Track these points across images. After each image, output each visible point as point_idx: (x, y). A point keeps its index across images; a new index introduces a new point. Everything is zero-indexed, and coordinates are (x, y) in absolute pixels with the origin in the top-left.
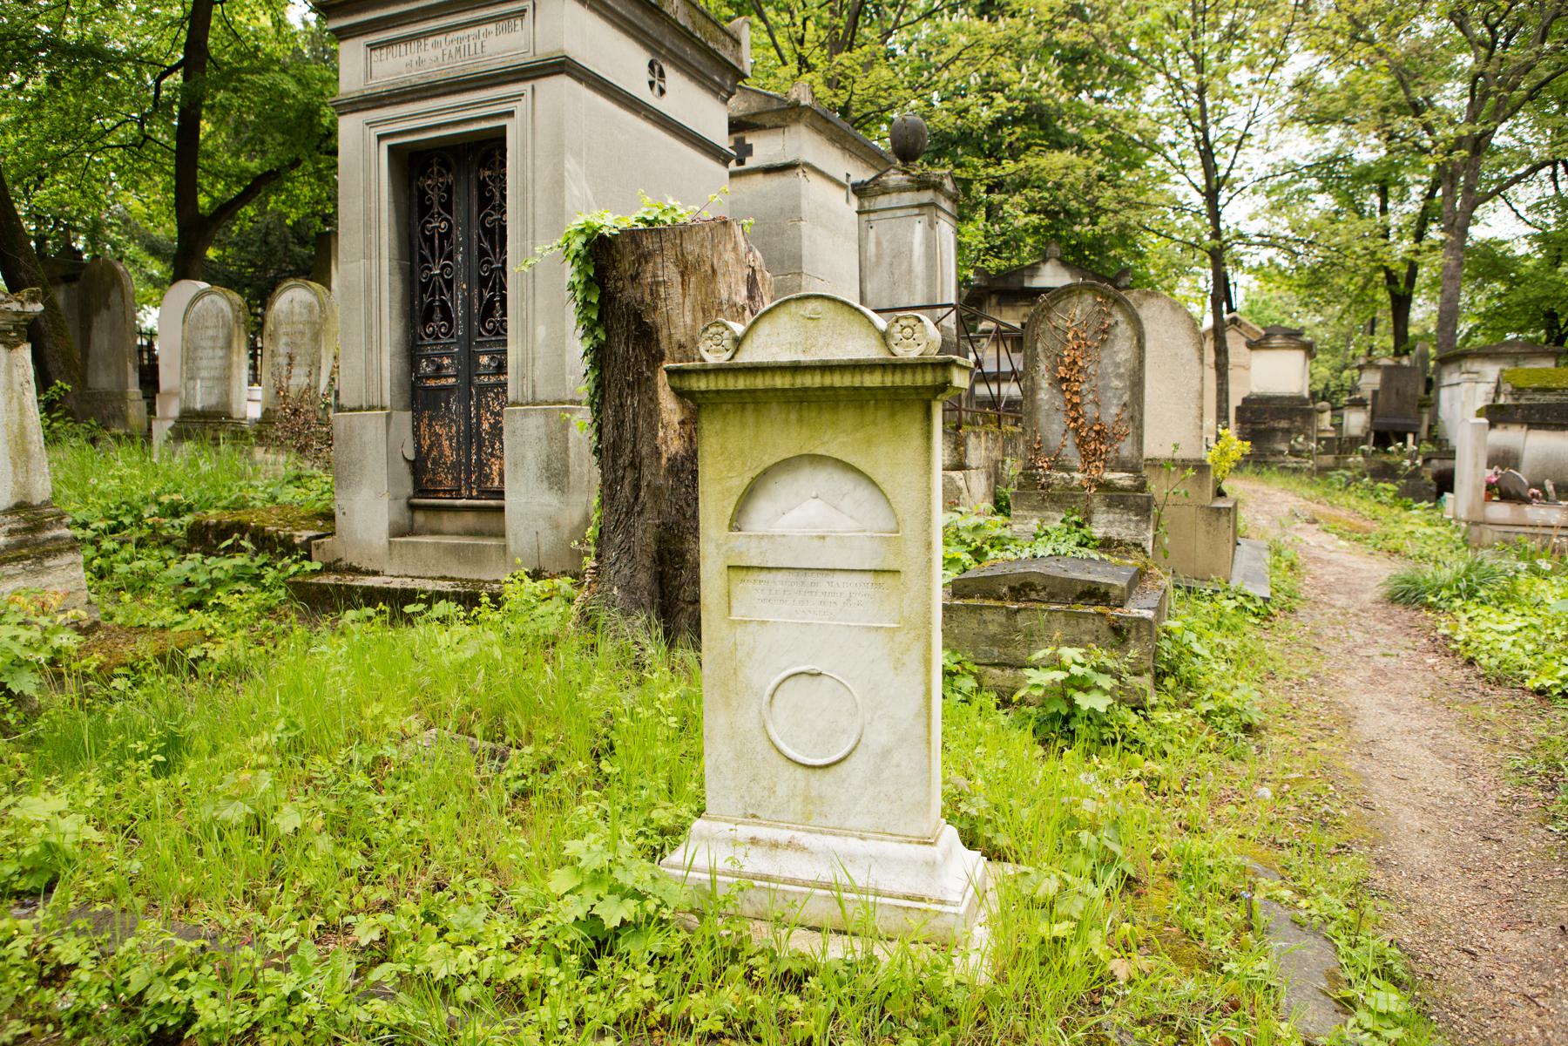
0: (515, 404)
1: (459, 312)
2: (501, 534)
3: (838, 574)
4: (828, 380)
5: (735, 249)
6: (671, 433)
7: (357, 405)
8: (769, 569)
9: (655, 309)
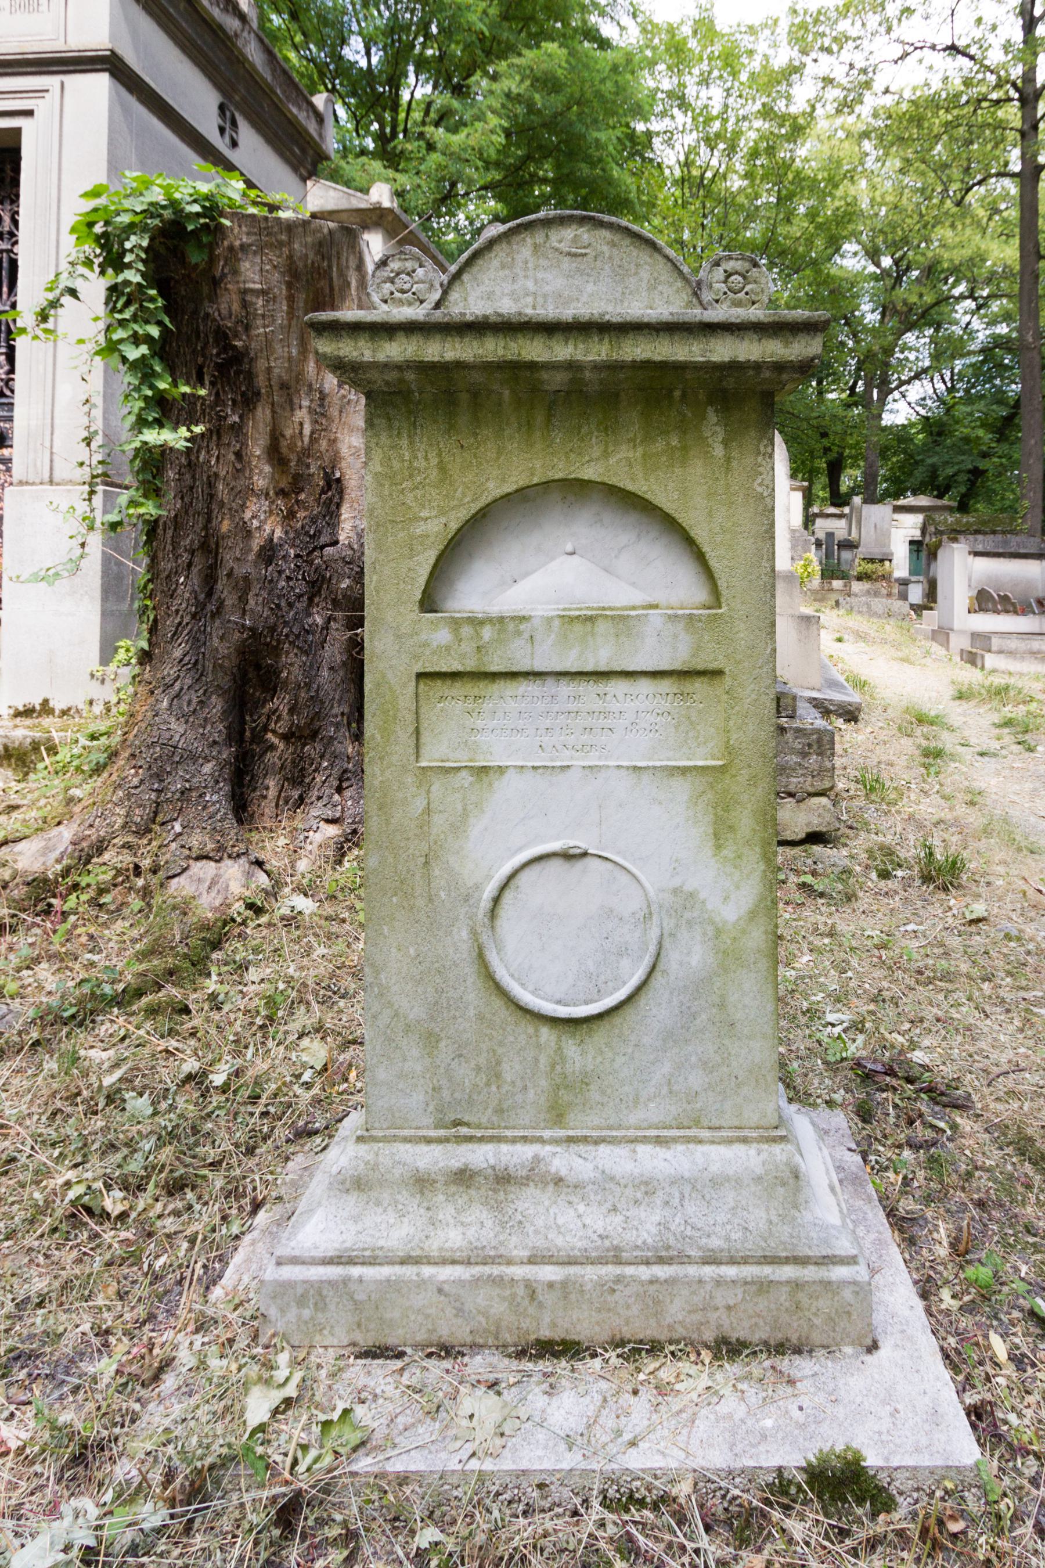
0: (21, 483)
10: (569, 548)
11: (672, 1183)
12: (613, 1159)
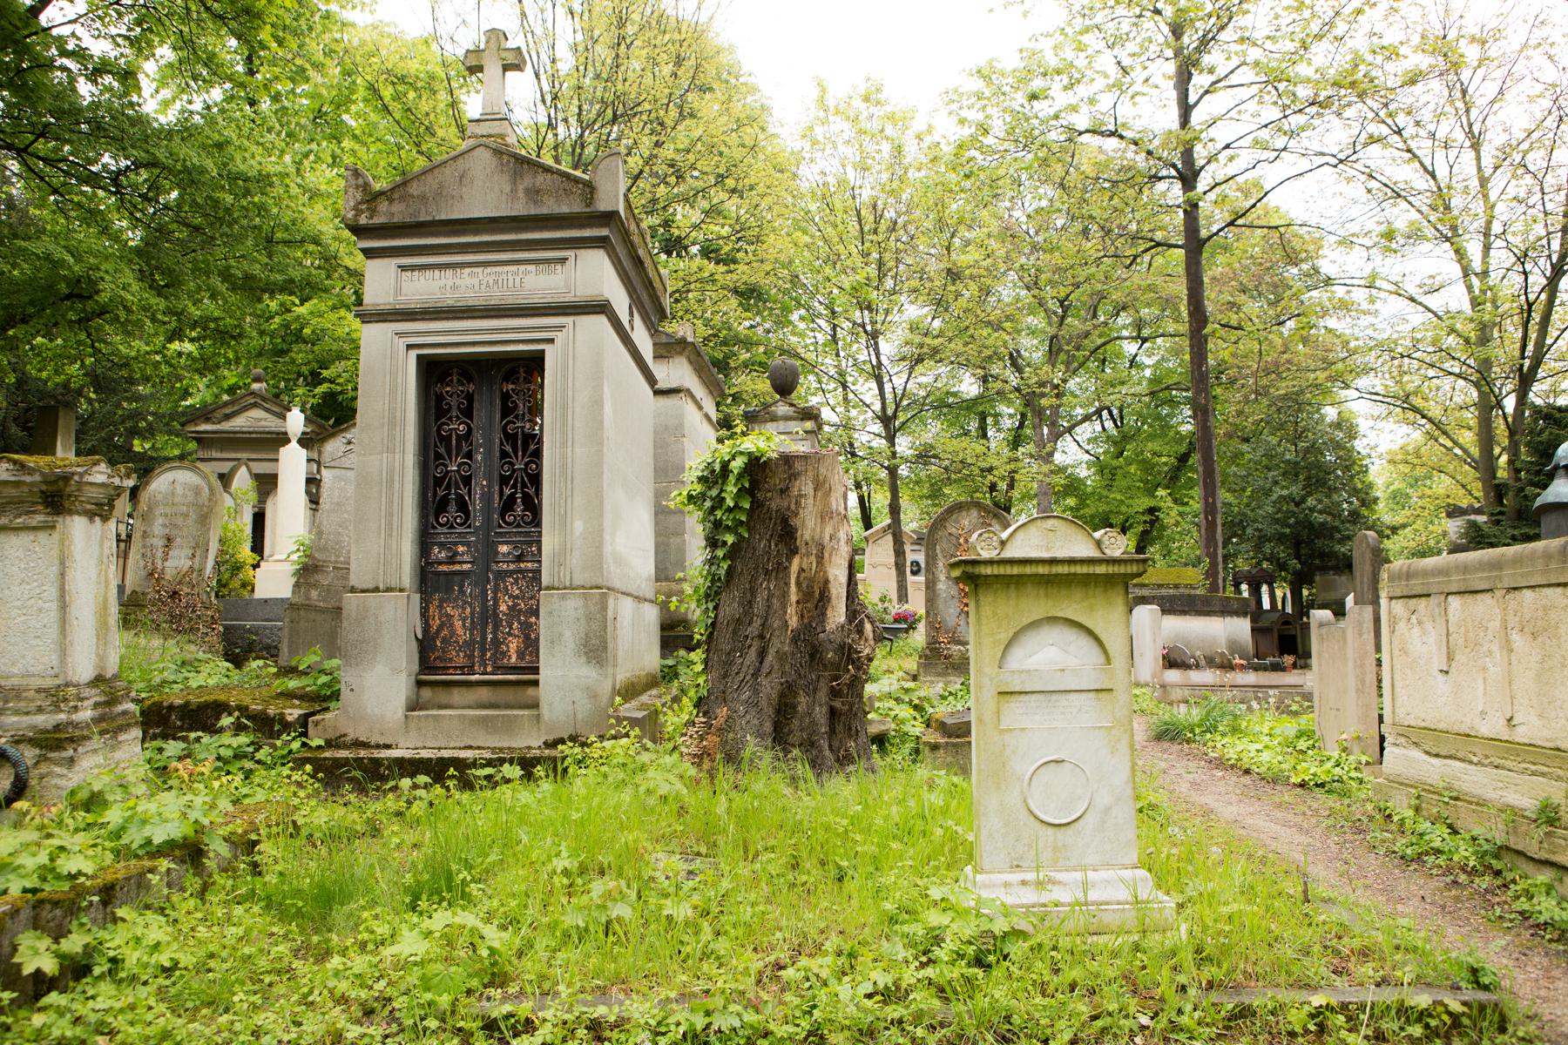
0: (548, 588)
1: (477, 505)
2: (535, 705)
3: (1074, 696)
7: (371, 586)
9: (797, 514)
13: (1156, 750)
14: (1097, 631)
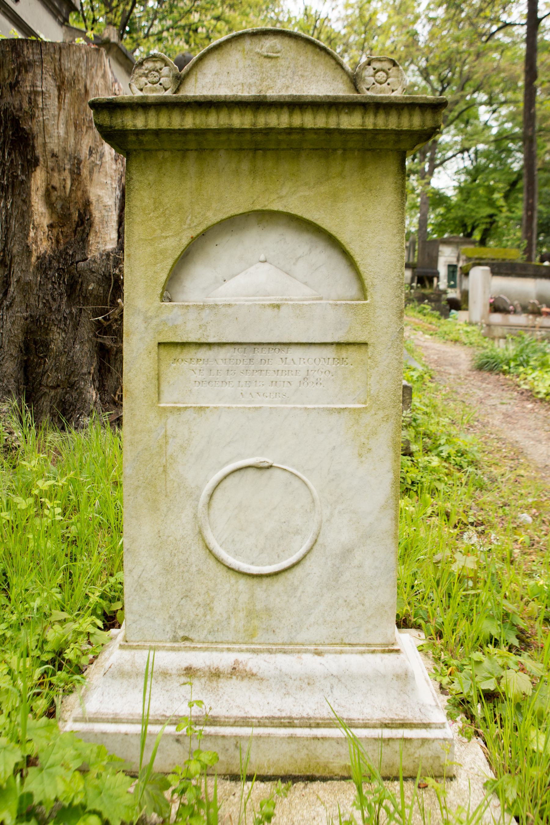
3: (295, 353)
4: (298, 120)
5: (104, 76)
6: (41, 235)
8: (210, 345)
9: (32, 117)
10: (262, 258)
11: (325, 678)
12: (285, 662)
13: (476, 378)
14: (344, 238)
